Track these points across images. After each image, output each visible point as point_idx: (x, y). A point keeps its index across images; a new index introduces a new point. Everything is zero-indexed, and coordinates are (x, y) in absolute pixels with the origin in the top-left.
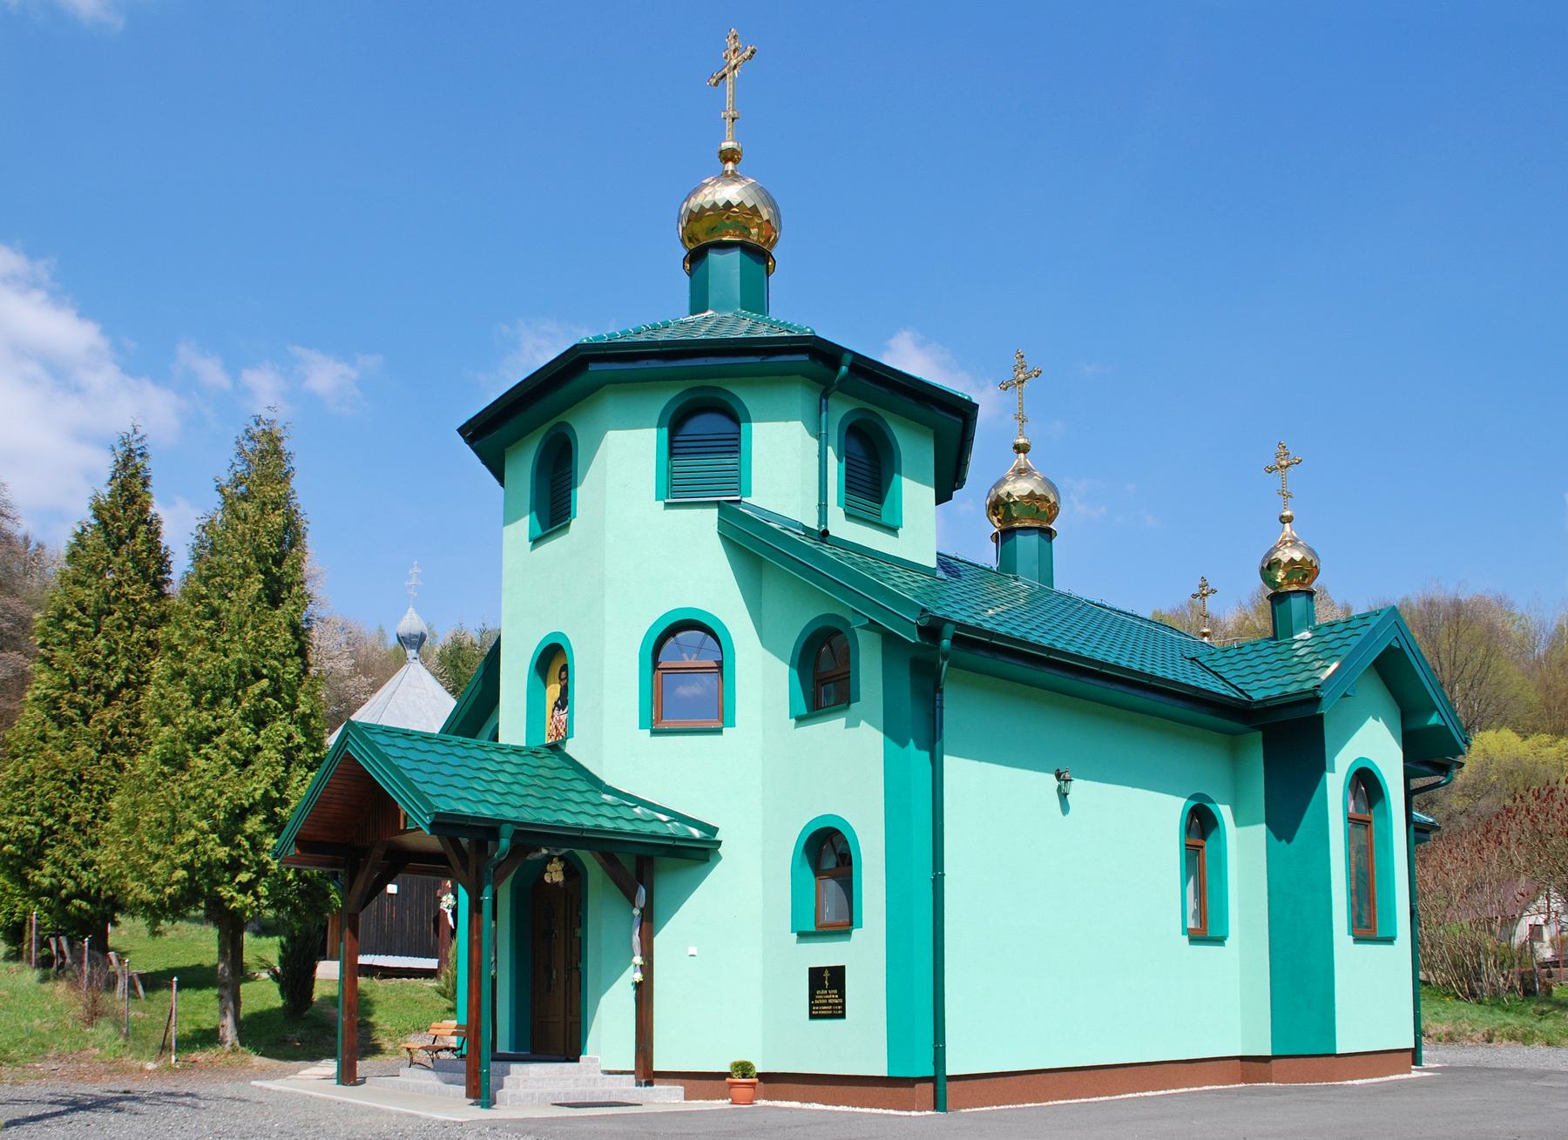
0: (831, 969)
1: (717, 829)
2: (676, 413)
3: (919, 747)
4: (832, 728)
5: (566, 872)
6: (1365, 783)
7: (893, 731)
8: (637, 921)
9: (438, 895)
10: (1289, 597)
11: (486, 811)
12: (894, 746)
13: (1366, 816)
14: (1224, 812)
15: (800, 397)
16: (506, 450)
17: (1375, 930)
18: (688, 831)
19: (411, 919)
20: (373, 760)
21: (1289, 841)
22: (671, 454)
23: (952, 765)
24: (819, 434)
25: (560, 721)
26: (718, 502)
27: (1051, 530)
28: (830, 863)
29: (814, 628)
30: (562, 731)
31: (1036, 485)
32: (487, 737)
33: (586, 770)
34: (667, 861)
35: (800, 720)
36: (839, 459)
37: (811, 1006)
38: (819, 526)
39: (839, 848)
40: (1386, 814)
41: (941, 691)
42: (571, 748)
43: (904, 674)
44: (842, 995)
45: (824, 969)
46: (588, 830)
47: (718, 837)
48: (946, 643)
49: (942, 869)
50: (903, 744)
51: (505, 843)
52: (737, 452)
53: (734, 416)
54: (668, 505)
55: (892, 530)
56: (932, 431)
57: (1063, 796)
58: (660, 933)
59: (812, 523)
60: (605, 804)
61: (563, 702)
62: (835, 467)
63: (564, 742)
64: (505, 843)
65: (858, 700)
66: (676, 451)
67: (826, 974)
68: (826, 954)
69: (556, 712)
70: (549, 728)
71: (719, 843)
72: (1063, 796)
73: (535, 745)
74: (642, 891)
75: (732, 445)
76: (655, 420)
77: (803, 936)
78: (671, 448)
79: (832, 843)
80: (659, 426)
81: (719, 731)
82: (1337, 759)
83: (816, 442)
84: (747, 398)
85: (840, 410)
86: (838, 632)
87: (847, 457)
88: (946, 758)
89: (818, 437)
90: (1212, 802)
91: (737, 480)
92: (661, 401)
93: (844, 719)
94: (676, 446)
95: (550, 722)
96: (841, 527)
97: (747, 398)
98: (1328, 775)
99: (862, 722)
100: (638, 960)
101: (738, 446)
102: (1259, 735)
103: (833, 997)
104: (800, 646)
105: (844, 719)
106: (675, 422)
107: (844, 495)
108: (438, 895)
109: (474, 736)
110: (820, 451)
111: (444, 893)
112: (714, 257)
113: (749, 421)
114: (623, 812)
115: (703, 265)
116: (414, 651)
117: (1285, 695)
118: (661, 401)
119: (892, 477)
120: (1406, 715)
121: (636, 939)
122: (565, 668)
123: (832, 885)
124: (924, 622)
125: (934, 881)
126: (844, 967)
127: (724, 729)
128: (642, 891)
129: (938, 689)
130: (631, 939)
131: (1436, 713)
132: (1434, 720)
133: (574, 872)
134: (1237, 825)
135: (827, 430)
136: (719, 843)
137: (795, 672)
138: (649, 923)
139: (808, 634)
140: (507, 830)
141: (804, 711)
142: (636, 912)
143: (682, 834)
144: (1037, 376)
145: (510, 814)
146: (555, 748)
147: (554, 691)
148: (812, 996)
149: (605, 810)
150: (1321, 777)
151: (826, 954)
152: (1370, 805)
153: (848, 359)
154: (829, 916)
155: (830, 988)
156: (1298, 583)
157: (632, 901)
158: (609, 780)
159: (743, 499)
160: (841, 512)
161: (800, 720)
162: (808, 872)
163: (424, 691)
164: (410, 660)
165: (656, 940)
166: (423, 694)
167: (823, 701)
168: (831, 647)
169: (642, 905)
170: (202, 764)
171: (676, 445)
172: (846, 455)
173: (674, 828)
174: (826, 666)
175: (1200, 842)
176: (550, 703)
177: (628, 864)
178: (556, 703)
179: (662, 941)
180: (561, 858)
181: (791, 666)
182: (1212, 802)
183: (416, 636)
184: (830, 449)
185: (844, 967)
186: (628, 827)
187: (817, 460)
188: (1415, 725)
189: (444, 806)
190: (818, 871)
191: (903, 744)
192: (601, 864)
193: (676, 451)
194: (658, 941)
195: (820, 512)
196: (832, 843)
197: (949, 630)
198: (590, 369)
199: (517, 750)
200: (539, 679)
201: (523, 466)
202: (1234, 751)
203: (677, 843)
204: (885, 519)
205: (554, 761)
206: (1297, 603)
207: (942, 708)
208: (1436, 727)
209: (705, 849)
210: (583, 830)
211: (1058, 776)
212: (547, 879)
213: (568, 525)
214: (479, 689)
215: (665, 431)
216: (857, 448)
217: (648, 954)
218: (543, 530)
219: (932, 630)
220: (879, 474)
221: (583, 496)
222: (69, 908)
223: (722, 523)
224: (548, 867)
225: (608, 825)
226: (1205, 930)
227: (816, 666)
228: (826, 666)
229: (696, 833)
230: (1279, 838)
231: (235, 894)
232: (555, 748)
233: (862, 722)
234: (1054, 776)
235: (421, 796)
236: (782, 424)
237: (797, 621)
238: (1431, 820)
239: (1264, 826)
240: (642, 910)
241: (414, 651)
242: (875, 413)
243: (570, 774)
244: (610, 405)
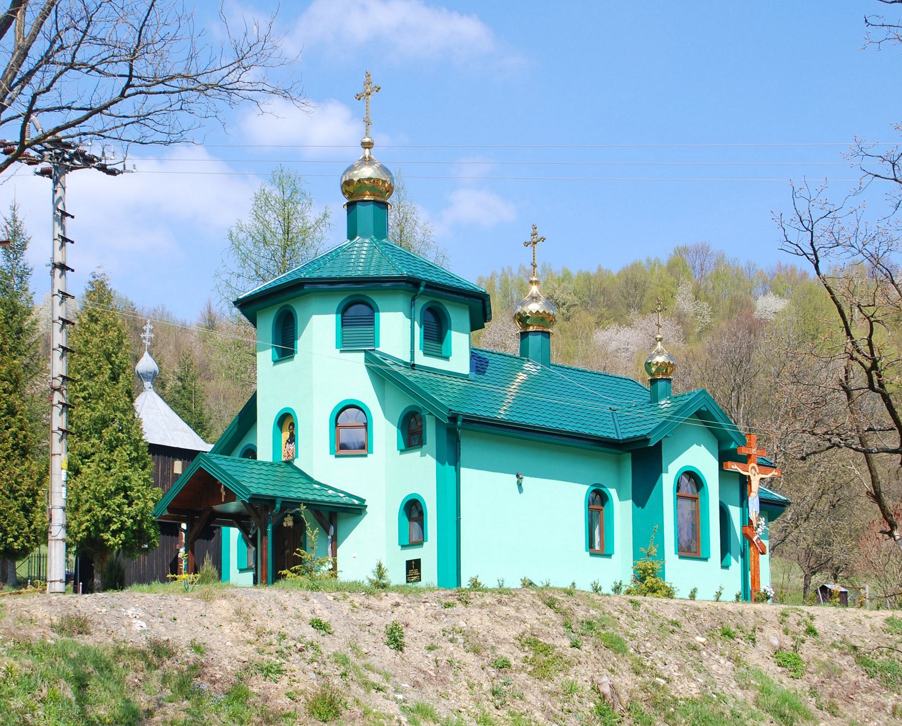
0: (415, 560)
1: (365, 500)
2: (342, 306)
3: (450, 464)
4: (415, 456)
5: (294, 521)
6: (693, 477)
7: (440, 459)
8: (330, 541)
9: (177, 548)
10: (657, 382)
11: (271, 493)
12: (439, 464)
13: (696, 496)
14: (612, 493)
15: (402, 301)
16: (258, 312)
17: (699, 554)
18: (352, 501)
19: (157, 565)
20: (219, 473)
21: (643, 507)
22: (343, 326)
23: (464, 471)
24: (411, 317)
25: (290, 449)
26: (365, 350)
27: (549, 333)
28: (415, 515)
29: (407, 411)
30: (291, 454)
31: (540, 307)
32: (238, 455)
33: (305, 473)
34: (344, 514)
35: (402, 451)
36: (421, 327)
37: (407, 577)
38: (411, 361)
39: (419, 509)
40: (706, 495)
41: (460, 442)
42: (296, 463)
43: (444, 432)
44: (420, 571)
45: (412, 561)
46: (311, 501)
47: (366, 504)
48: (459, 423)
49: (460, 516)
50: (443, 464)
51: (278, 506)
52: (372, 325)
53: (373, 309)
54: (342, 351)
55: (447, 358)
56: (468, 306)
57: (520, 485)
58: (341, 546)
59: (408, 360)
60: (315, 489)
61: (292, 439)
62: (418, 331)
63: (293, 460)
64: (278, 506)
65: (426, 444)
66: (344, 324)
67: (413, 563)
68: (413, 554)
69: (287, 445)
70: (284, 452)
71: (366, 506)
72: (520, 485)
73: (277, 461)
74: (332, 528)
75: (370, 321)
76: (335, 310)
77: (403, 547)
78: (342, 322)
79: (416, 507)
80: (337, 313)
81: (366, 456)
82: (670, 467)
83: (410, 320)
84: (378, 301)
85: (420, 304)
86: (418, 413)
87: (424, 326)
88: (461, 469)
89: (411, 319)
90: (604, 487)
91: (373, 339)
92: (336, 302)
93: (420, 452)
94: (345, 322)
95: (285, 450)
96: (421, 359)
97: (378, 301)
98: (664, 475)
99: (427, 455)
100: (331, 559)
101: (374, 322)
102: (630, 454)
103: (416, 573)
104: (402, 418)
105: (420, 452)
106: (343, 311)
107: (423, 342)
108: (177, 548)
109: (229, 455)
110: (411, 325)
111: (181, 547)
112: (359, 207)
113: (378, 311)
114: (323, 492)
115: (354, 210)
116: (149, 383)
117: (635, 437)
118: (336, 302)
119: (447, 331)
120: (720, 444)
121: (330, 549)
122: (292, 424)
123: (416, 525)
124: (450, 415)
125: (457, 521)
126: (420, 559)
127: (368, 455)
128: (332, 528)
129: (458, 441)
130: (327, 549)
131: (734, 442)
132: (733, 446)
133: (298, 520)
134: (620, 500)
135: (414, 316)
136: (366, 506)
137: (400, 431)
138: (335, 542)
139: (405, 414)
140: (279, 501)
141: (403, 448)
142: (330, 537)
143: (350, 503)
144: (543, 241)
145: (279, 494)
146: (289, 463)
147: (286, 435)
148: (407, 573)
149: (315, 492)
150: (658, 477)
151: (413, 554)
152: (698, 490)
153: (423, 284)
154: (415, 538)
155: (415, 568)
156: (663, 374)
157: (328, 533)
158: (316, 478)
159: (376, 349)
160: (421, 352)
161: (402, 451)
162: (406, 519)
163: (158, 411)
164: (147, 389)
165: (338, 550)
166: (158, 413)
167: (413, 443)
168: (415, 419)
169: (332, 534)
170: (88, 471)
171: (344, 321)
172: (424, 324)
173: (346, 500)
174: (413, 427)
175: (600, 507)
176: (284, 440)
177: (326, 516)
178: (287, 441)
179: (340, 550)
180: (291, 515)
181: (398, 428)
182: (604, 487)
183: (151, 373)
184: (416, 323)
185: (420, 559)
186: (327, 499)
187: (410, 329)
188: (724, 448)
189: (254, 491)
190: (410, 519)
191: (443, 464)
192: (314, 516)
193: (344, 324)
194: (339, 550)
195: (411, 354)
196: (416, 507)
197: (460, 418)
198: (305, 288)
199: (264, 464)
200: (278, 429)
201: (267, 323)
202: (619, 462)
203: (348, 506)
204: (444, 354)
205: (290, 469)
206: (661, 385)
207: (460, 449)
208: (733, 449)
209: (360, 509)
210: (309, 501)
211: (518, 476)
212: (285, 525)
213: (293, 357)
214: (236, 429)
215: (340, 315)
216: (431, 319)
217: (334, 554)
218: (279, 358)
219: (453, 418)
220: (441, 330)
221: (301, 344)
222: (77, 538)
223: (366, 360)
224: (285, 519)
225: (319, 498)
226: (603, 551)
227: (409, 426)
228: (413, 427)
229: (356, 502)
230: (638, 506)
231: (110, 537)
232: (289, 463)
233: (427, 455)
234: (515, 476)
235: (244, 487)
236: (394, 313)
237: (401, 406)
238: (786, 499)
239: (631, 501)
240: (332, 536)
241: (149, 383)
242: (439, 302)
243: (297, 476)
244: (315, 303)
